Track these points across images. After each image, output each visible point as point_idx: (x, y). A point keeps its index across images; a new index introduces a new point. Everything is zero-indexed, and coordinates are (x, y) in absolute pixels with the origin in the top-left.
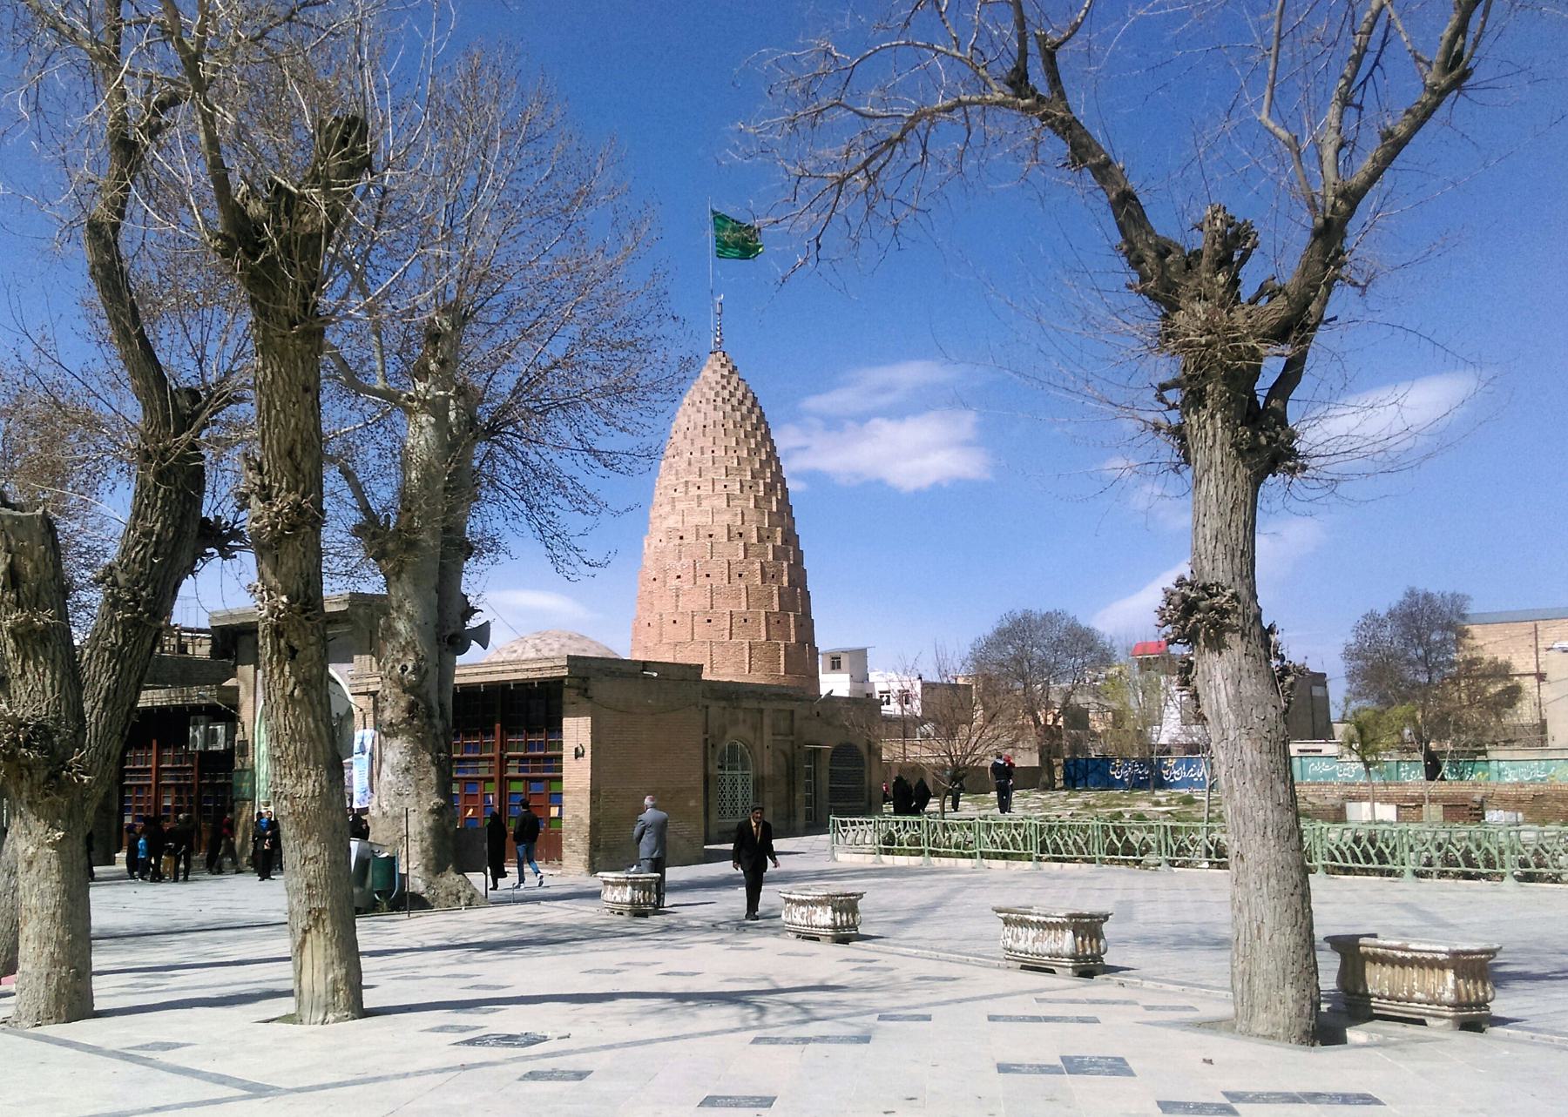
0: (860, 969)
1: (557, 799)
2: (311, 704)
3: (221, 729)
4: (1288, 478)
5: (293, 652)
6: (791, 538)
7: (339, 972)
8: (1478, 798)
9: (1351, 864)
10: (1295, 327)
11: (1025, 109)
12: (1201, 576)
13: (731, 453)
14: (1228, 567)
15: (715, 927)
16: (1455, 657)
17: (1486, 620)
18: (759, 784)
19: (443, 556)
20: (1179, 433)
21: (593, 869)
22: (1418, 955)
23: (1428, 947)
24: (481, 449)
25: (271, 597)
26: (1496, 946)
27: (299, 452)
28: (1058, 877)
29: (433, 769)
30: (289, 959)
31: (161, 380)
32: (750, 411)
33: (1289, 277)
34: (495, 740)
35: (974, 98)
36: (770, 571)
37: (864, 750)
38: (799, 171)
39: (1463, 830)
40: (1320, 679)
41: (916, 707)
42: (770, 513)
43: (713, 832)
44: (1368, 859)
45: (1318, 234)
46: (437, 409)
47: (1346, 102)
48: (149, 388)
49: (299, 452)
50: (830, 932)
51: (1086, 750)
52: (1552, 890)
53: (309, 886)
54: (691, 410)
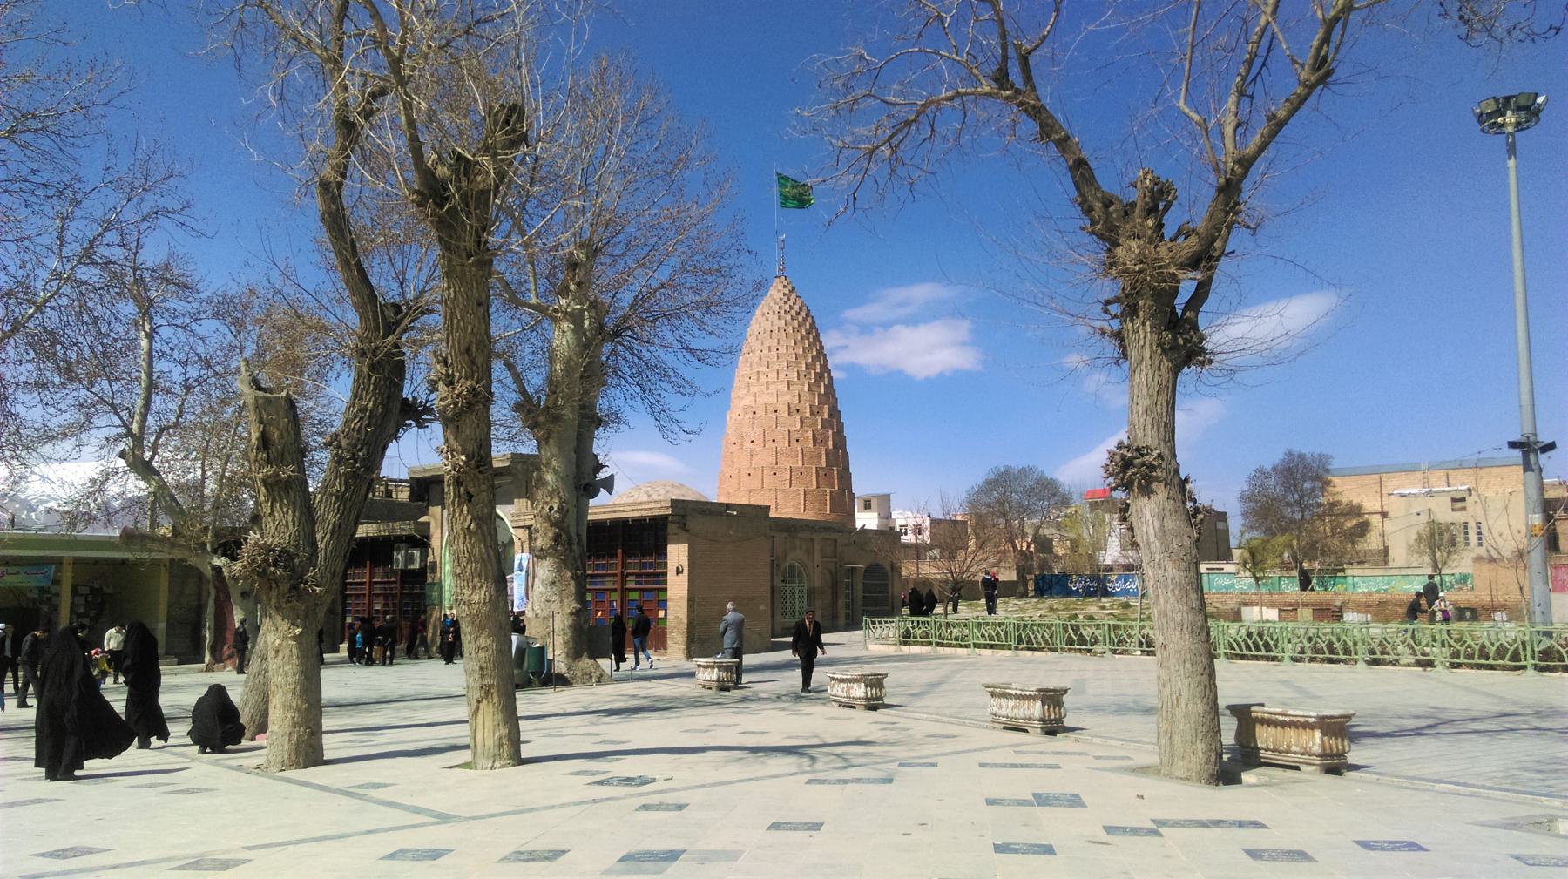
1: (663, 604)
3: (416, 553)
5: (470, 497)
6: (834, 413)
7: (504, 731)
10: (1204, 258)
14: (1154, 433)
15: (779, 698)
16: (1322, 500)
17: (1343, 473)
18: (812, 593)
19: (580, 426)
24: (607, 347)
28: (1031, 662)
31: (373, 297)
32: (805, 320)
34: (618, 561)
36: (819, 437)
37: (888, 568)
38: (840, 144)
39: (1327, 627)
40: (1222, 516)
43: (778, 628)
44: (1258, 648)
45: (1220, 190)
46: (576, 318)
47: (1241, 94)
51: (1051, 568)
54: (761, 319)
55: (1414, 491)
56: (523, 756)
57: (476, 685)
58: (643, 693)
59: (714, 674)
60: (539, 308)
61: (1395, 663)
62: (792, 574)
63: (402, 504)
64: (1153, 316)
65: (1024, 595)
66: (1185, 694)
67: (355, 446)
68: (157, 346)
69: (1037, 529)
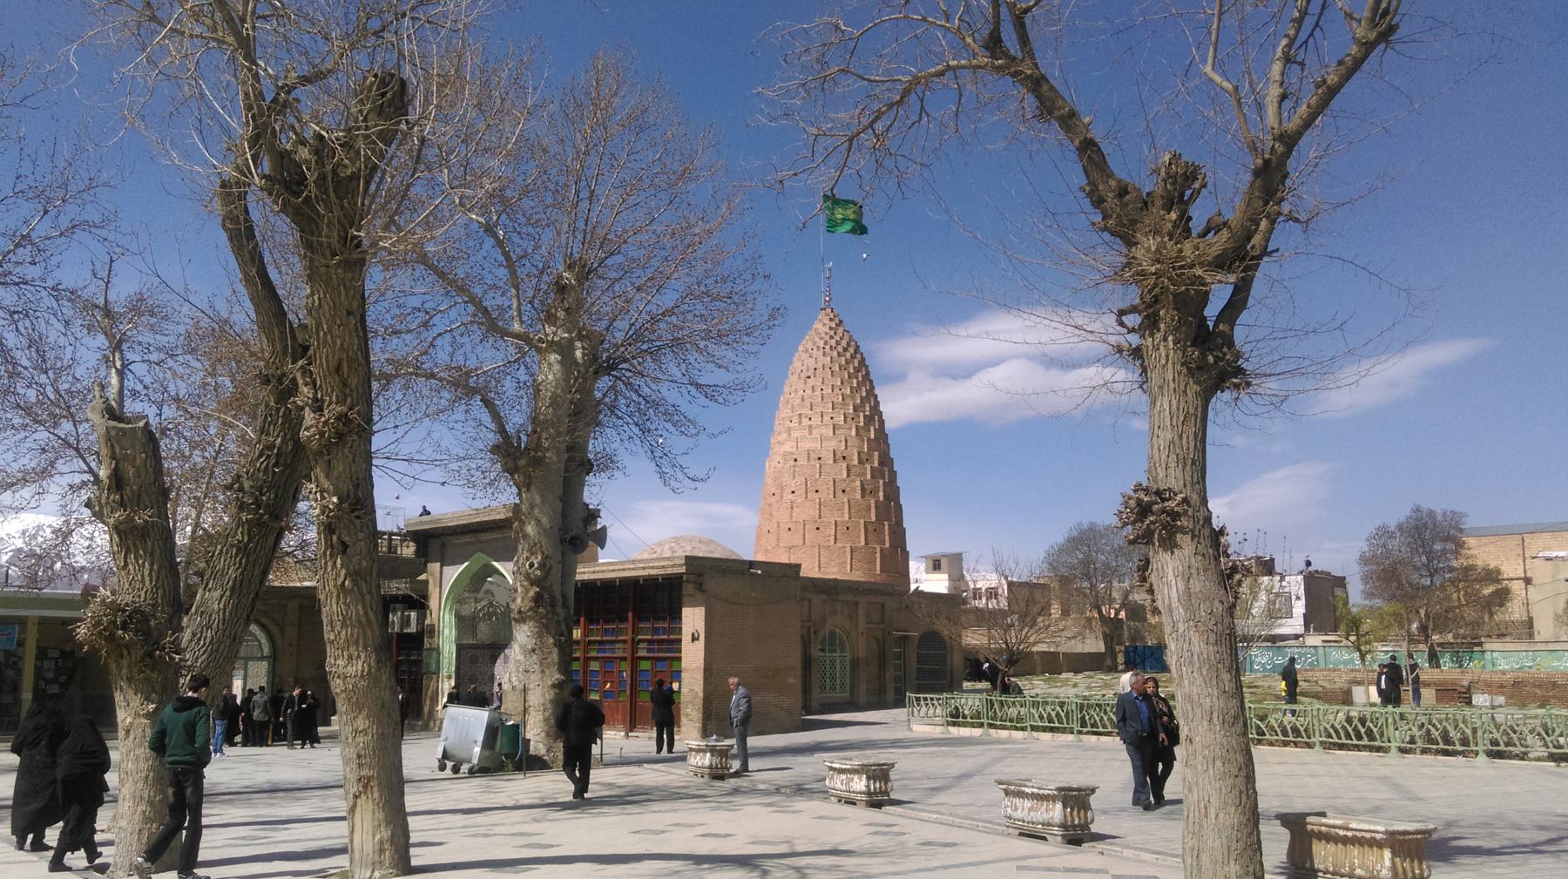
0: (876, 833)
1: (677, 675)
2: (361, 594)
3: (413, 615)
4: (1235, 394)
5: (345, 546)
6: (886, 461)
7: (385, 833)
8: (1465, 683)
9: (1344, 741)
10: (1241, 258)
11: (998, 69)
12: (1156, 481)
13: (836, 391)
14: (1179, 474)
15: (778, 791)
16: (1455, 564)
17: (1480, 533)
18: (855, 663)
19: (566, 471)
20: (1137, 353)
21: (705, 734)
22: (1358, 834)
23: (1366, 827)
24: (604, 382)
25: (323, 498)
26: (1431, 826)
27: (345, 369)
28: (1091, 749)
29: (556, 650)
30: (343, 819)
31: (282, 314)
32: (853, 357)
33: (1234, 213)
34: (628, 626)
35: (963, 62)
36: (868, 488)
38: (815, 131)
39: (1451, 710)
40: (1340, 582)
41: (1004, 604)
42: (869, 440)
43: (815, 704)
44: (1359, 737)
45: (1257, 173)
46: (565, 349)
47: (1288, 60)
48: (270, 323)
49: (345, 369)
50: (864, 797)
51: (1143, 639)
52: (1520, 767)
53: (359, 756)
55: (1561, 554)
56: (414, 862)
57: (353, 777)
58: (622, 781)
59: (707, 759)
60: (524, 338)
61: (1523, 757)
62: (832, 642)
63: (407, 561)
64: (1176, 329)
65: (1113, 669)
66: (1215, 802)
67: (260, 489)
68: (130, 383)
69: (1126, 594)
